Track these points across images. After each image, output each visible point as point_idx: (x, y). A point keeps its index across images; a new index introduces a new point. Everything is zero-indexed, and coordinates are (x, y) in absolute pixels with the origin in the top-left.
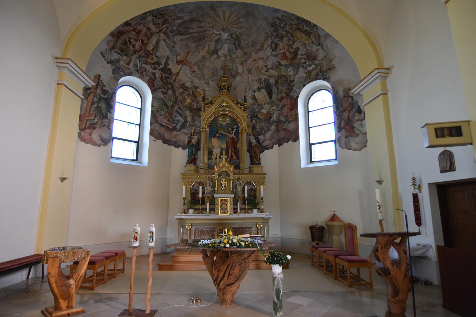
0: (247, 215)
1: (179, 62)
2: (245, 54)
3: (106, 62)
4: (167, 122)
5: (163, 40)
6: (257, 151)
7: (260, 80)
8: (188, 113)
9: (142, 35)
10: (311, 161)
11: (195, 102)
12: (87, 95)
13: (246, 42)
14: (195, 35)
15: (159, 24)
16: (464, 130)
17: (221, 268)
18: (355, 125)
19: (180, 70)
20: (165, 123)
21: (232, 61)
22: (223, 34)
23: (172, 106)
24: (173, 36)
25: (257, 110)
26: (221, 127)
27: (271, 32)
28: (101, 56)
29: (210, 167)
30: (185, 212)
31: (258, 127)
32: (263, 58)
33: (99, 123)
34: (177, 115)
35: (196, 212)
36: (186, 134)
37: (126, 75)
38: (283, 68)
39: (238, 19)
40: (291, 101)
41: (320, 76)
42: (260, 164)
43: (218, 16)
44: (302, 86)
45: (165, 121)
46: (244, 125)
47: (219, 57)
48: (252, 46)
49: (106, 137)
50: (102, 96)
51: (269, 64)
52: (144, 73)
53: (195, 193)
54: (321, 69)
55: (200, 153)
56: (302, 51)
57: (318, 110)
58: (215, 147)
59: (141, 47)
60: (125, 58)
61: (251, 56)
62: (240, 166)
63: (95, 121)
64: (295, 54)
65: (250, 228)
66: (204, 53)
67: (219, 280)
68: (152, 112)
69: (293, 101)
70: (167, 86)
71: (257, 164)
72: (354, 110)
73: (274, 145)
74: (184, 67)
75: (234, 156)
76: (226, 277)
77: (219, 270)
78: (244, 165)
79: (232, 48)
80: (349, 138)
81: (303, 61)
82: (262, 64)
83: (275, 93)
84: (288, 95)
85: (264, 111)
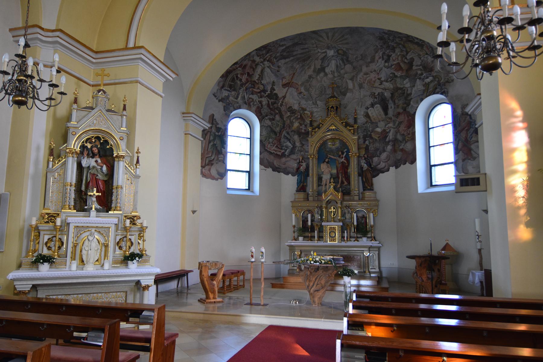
0: (356, 243)
2: (354, 68)
3: (217, 101)
4: (276, 149)
5: (268, 67)
6: (369, 176)
7: (373, 95)
8: (296, 137)
9: (247, 68)
10: (432, 185)
11: (303, 126)
12: (204, 135)
13: (355, 57)
14: (299, 56)
15: (263, 54)
16: (482, 181)
18: (473, 147)
19: (286, 93)
20: (274, 150)
22: (328, 51)
23: (280, 131)
24: (278, 61)
25: (371, 129)
26: (331, 151)
27: (381, 44)
28: (213, 97)
30: (296, 239)
31: (372, 148)
32: (375, 71)
33: (215, 159)
34: (286, 141)
37: (235, 109)
38: (398, 80)
39: (343, 36)
40: (408, 117)
41: (438, 90)
42: (373, 190)
43: (321, 36)
44: (419, 101)
45: (274, 148)
46: (354, 149)
47: (326, 75)
49: (222, 171)
50: (217, 134)
51: (383, 76)
52: (252, 104)
53: (305, 221)
54: (439, 81)
55: (309, 179)
57: (438, 124)
58: (324, 173)
59: (247, 79)
60: (233, 93)
62: (351, 192)
63: (213, 158)
64: (410, 64)
65: (358, 256)
66: (310, 72)
67: (310, 288)
69: (410, 118)
71: (369, 190)
72: (472, 130)
73: (391, 168)
75: (345, 182)
76: (315, 286)
77: (310, 281)
78: (355, 192)
79: (340, 64)
80: (466, 161)
81: (419, 72)
82: (375, 77)
83: (391, 108)
85: (379, 130)
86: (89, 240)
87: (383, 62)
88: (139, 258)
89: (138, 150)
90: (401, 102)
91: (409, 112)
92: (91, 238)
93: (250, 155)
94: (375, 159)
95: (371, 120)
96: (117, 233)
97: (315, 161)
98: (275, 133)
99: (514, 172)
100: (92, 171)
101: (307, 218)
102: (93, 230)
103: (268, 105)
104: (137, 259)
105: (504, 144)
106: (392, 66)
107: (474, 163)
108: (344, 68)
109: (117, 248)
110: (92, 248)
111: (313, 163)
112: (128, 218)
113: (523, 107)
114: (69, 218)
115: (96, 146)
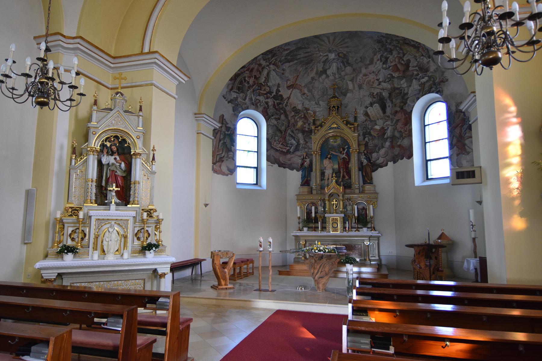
1: (289, 87)
2: (354, 70)
3: (227, 102)
4: (281, 146)
5: (273, 70)
6: (369, 170)
8: (300, 135)
10: (428, 179)
11: (307, 124)
13: (354, 59)
14: (302, 59)
15: (268, 58)
17: (51, 65)
20: (280, 147)
21: (342, 78)
22: (330, 55)
23: (286, 130)
24: (282, 64)
25: (370, 127)
26: (333, 148)
29: (322, 188)
30: (301, 230)
31: (371, 144)
32: (373, 72)
34: (290, 138)
35: (310, 229)
36: (300, 156)
37: (243, 110)
38: (396, 80)
39: (344, 40)
40: (405, 115)
41: (433, 89)
46: (354, 145)
47: (328, 76)
48: (361, 62)
49: (231, 167)
50: (227, 133)
51: (381, 77)
52: (258, 104)
53: (309, 213)
54: (434, 81)
55: (313, 174)
56: (413, 63)
57: (433, 122)
59: (254, 82)
60: (241, 95)
61: (361, 72)
62: (352, 186)
63: (223, 155)
64: (407, 65)
65: (359, 245)
66: (313, 74)
67: (314, 275)
68: (268, 139)
70: (280, 111)
73: (389, 163)
74: (295, 91)
76: (319, 273)
77: (314, 269)
78: (356, 186)
79: (341, 66)
80: (460, 155)
81: (415, 73)
82: (374, 78)
83: (389, 106)
84: (402, 108)
85: (378, 127)
86: (109, 232)
87: (381, 64)
88: (156, 248)
89: (154, 148)
90: (398, 101)
91: (406, 110)
92: (111, 230)
93: (257, 152)
94: (375, 155)
95: (370, 118)
96: (135, 225)
97: (318, 157)
98: (281, 132)
99: (509, 165)
100: (112, 168)
101: (311, 210)
102: (113, 223)
103: (274, 106)
104: (154, 248)
105: (499, 139)
106: (389, 67)
107: (468, 157)
108: (344, 70)
109: (135, 239)
110: (112, 240)
111: (316, 159)
112: (145, 212)
113: (516, 103)
114: (90, 212)
115: (115, 145)
